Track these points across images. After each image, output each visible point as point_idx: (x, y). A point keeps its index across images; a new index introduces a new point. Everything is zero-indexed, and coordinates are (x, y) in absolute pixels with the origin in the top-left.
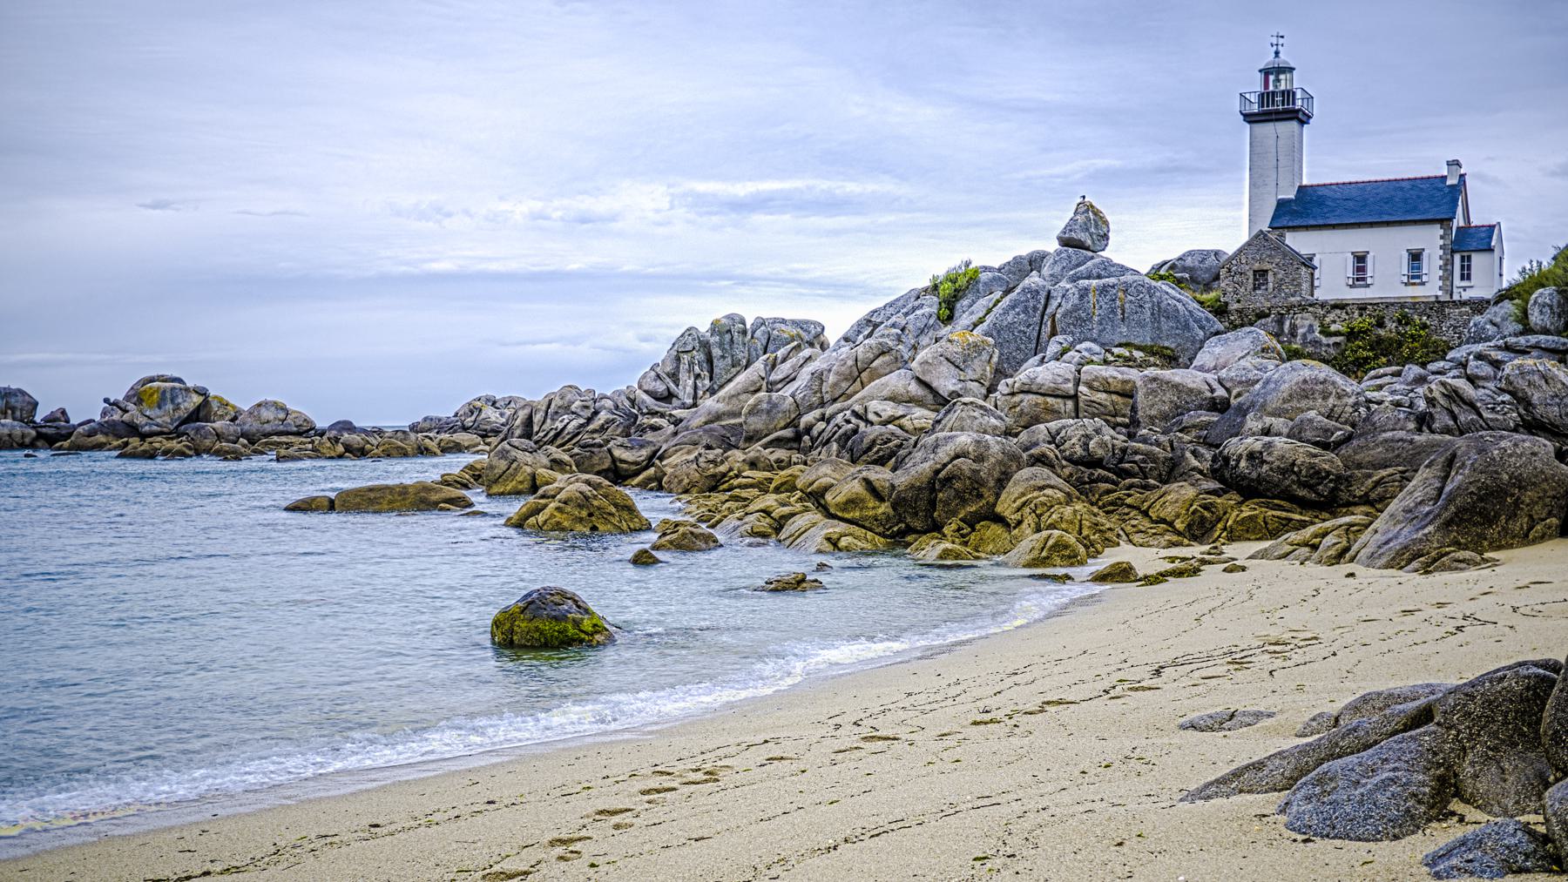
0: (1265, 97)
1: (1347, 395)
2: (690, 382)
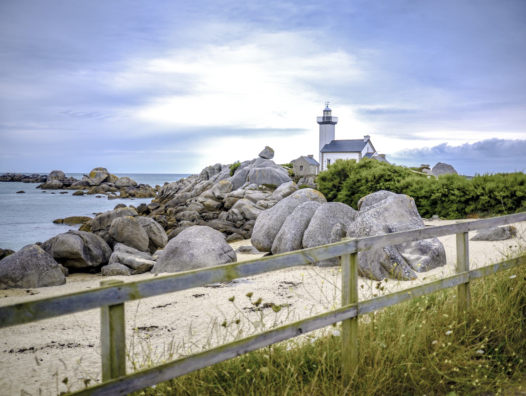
0: (324, 118)
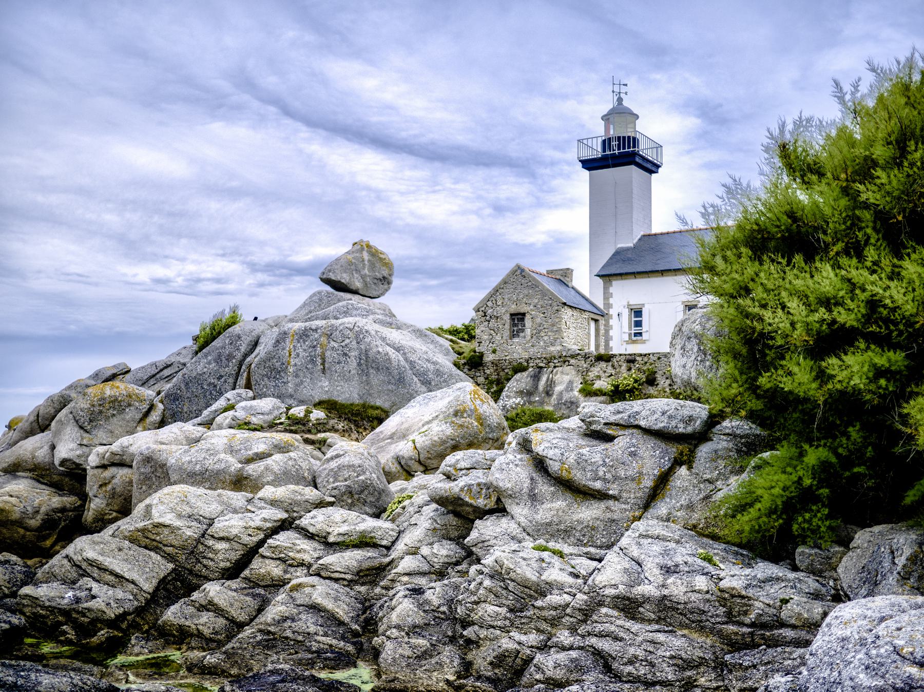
0: (606, 143)
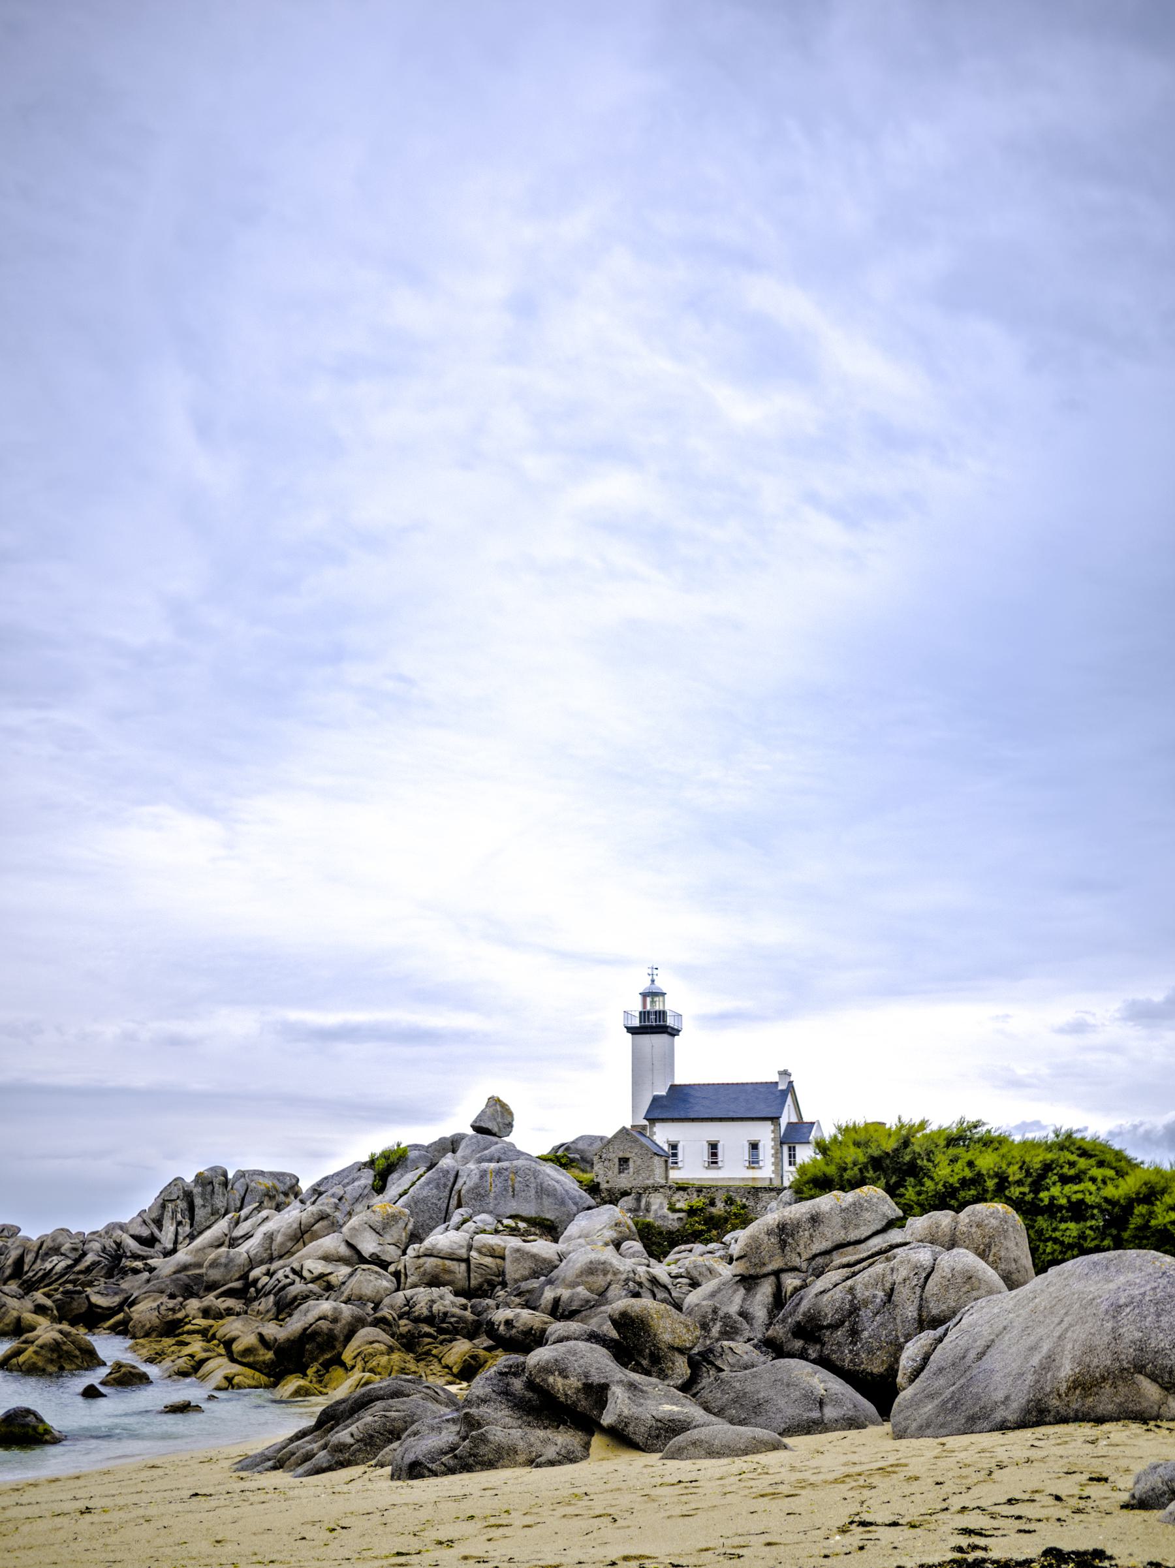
0: (644, 1015)
1: (620, 1272)
2: (172, 1229)
